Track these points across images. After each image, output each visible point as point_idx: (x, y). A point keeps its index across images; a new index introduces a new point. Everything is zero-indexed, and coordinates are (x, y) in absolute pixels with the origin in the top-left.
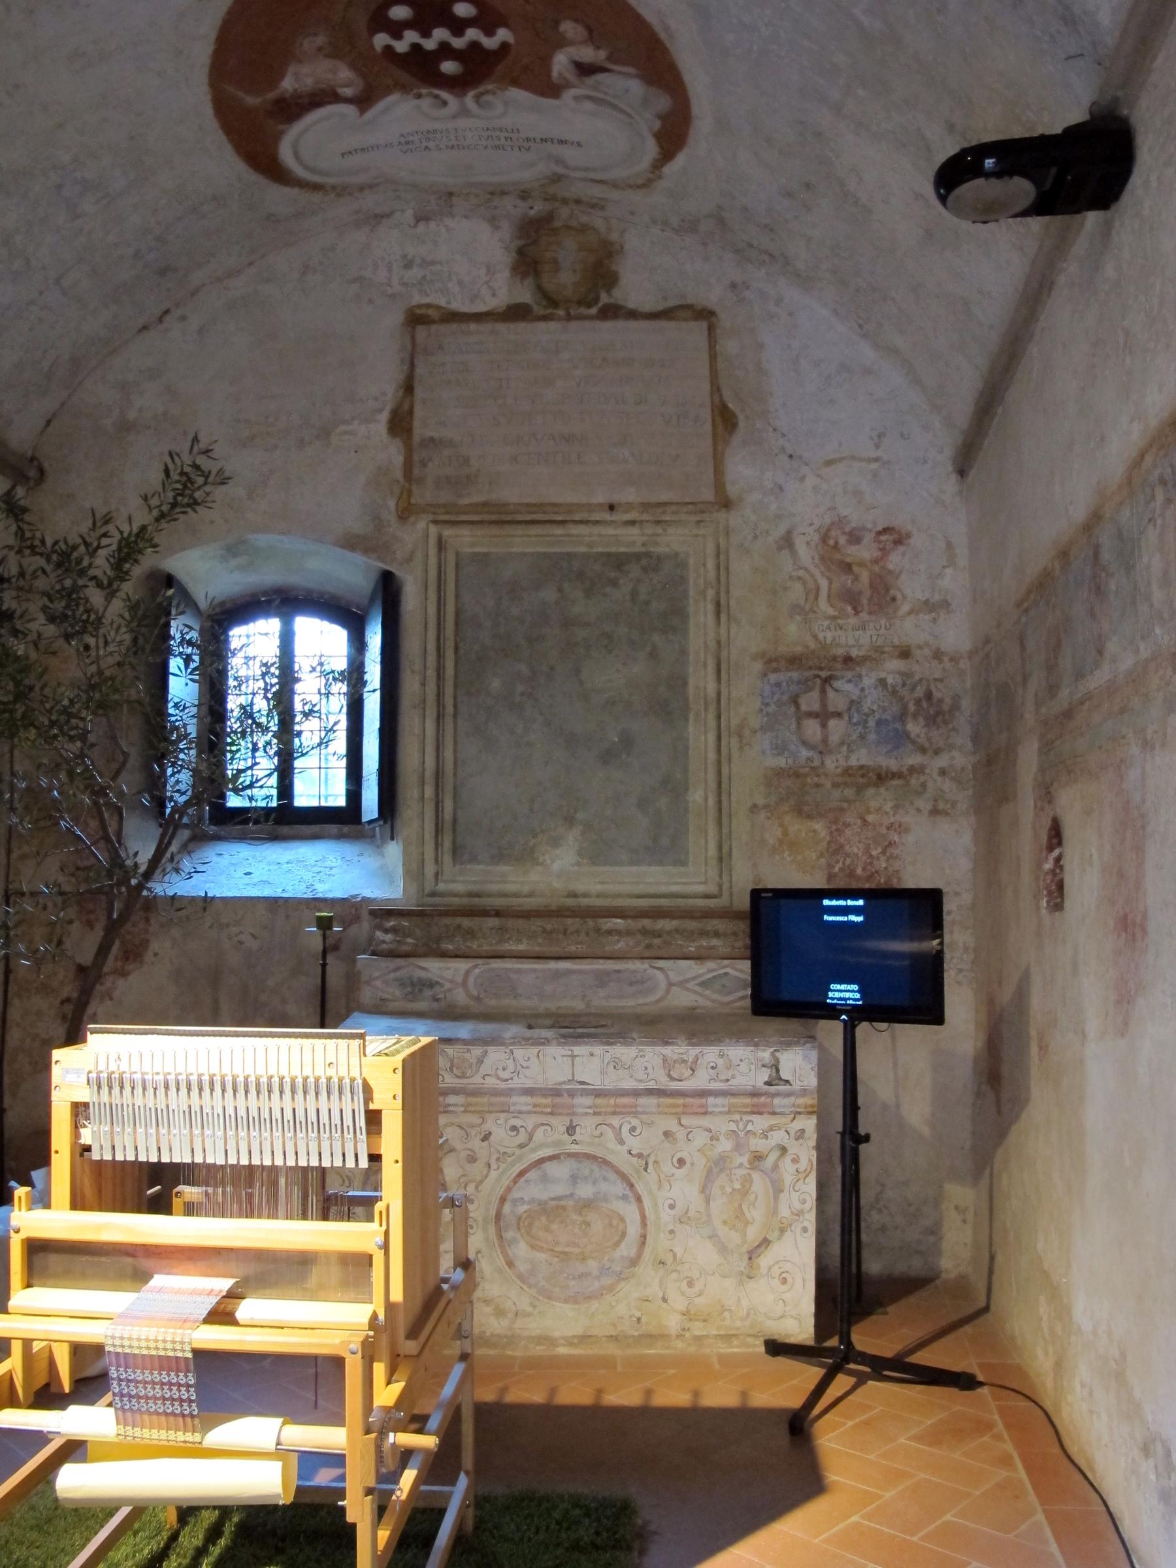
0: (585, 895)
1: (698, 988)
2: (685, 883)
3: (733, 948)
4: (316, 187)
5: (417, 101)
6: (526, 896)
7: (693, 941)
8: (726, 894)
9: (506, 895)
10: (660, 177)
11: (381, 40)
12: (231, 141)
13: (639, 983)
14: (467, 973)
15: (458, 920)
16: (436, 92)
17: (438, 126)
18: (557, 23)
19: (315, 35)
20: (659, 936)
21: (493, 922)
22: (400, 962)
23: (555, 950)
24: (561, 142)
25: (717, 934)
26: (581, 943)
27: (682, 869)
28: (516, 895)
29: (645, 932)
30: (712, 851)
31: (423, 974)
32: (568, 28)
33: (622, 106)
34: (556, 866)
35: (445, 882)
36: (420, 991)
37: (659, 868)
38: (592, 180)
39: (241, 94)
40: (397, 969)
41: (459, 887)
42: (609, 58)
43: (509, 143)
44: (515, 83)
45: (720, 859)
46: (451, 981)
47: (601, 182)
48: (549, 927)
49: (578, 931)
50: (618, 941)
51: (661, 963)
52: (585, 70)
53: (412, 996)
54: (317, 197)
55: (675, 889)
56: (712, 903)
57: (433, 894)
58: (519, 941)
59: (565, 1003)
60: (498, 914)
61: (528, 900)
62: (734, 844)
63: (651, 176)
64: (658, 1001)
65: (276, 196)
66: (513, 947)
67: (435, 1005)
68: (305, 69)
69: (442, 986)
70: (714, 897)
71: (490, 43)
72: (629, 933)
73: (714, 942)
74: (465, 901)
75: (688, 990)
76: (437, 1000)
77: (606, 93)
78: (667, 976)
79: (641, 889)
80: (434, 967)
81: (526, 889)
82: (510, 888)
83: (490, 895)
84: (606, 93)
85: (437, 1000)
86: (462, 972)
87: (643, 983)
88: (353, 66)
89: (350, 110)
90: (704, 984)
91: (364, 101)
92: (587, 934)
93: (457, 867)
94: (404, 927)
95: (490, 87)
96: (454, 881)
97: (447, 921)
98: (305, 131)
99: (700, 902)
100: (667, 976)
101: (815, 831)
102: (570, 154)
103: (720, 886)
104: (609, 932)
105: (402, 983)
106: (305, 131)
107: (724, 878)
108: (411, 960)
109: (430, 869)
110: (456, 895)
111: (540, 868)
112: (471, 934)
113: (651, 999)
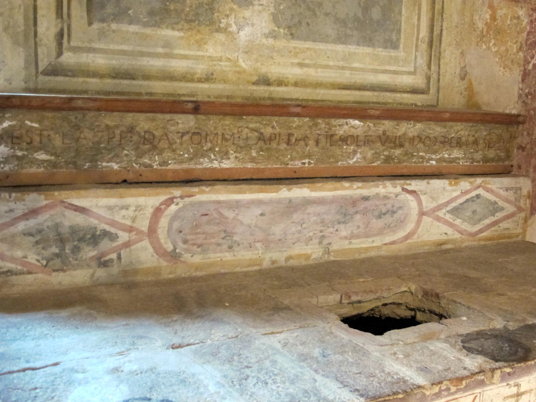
0: (280, 83)
1: (448, 217)
2: (395, 73)
3: (473, 160)
6: (200, 81)
7: (435, 152)
8: (432, 91)
9: (170, 77)
13: (390, 212)
14: (158, 212)
15: (130, 118)
20: (401, 146)
21: (186, 122)
22: (35, 200)
23: (272, 166)
25: (459, 144)
26: (309, 156)
27: (393, 53)
28: (186, 78)
29: (386, 140)
30: (424, 33)
31: (79, 220)
34: (244, 35)
35: (76, 50)
36: (76, 250)
37: (368, 50)
40: (34, 212)
41: (100, 61)
45: (431, 44)
46: (130, 229)
48: (268, 131)
49: (305, 138)
50: (355, 152)
51: (415, 185)
53: (61, 262)
55: (384, 79)
56: (419, 99)
57: (54, 71)
58: (225, 155)
59: (298, 250)
60: (196, 108)
61: (206, 86)
62: (445, 25)
64: (407, 238)
66: (216, 165)
67: (101, 273)
69: (113, 237)
70: (422, 92)
72: (368, 141)
73: (457, 153)
74: (109, 84)
75: (438, 219)
76: (105, 264)
78: (420, 203)
79: (346, 77)
80: (100, 206)
81: (200, 68)
82: (178, 66)
83: (147, 77)
85: (105, 264)
86: (149, 211)
87: (394, 212)
90: (455, 211)
92: (317, 142)
93: (96, 26)
94: (30, 129)
96: (90, 50)
97: (109, 120)
99: (408, 98)
100: (420, 203)
101: (518, 18)
103: (428, 78)
104: (344, 140)
105: (39, 237)
107: (433, 67)
108: (57, 194)
109: (47, 27)
110: (95, 74)
111: (221, 37)
112: (149, 143)
113: (401, 234)
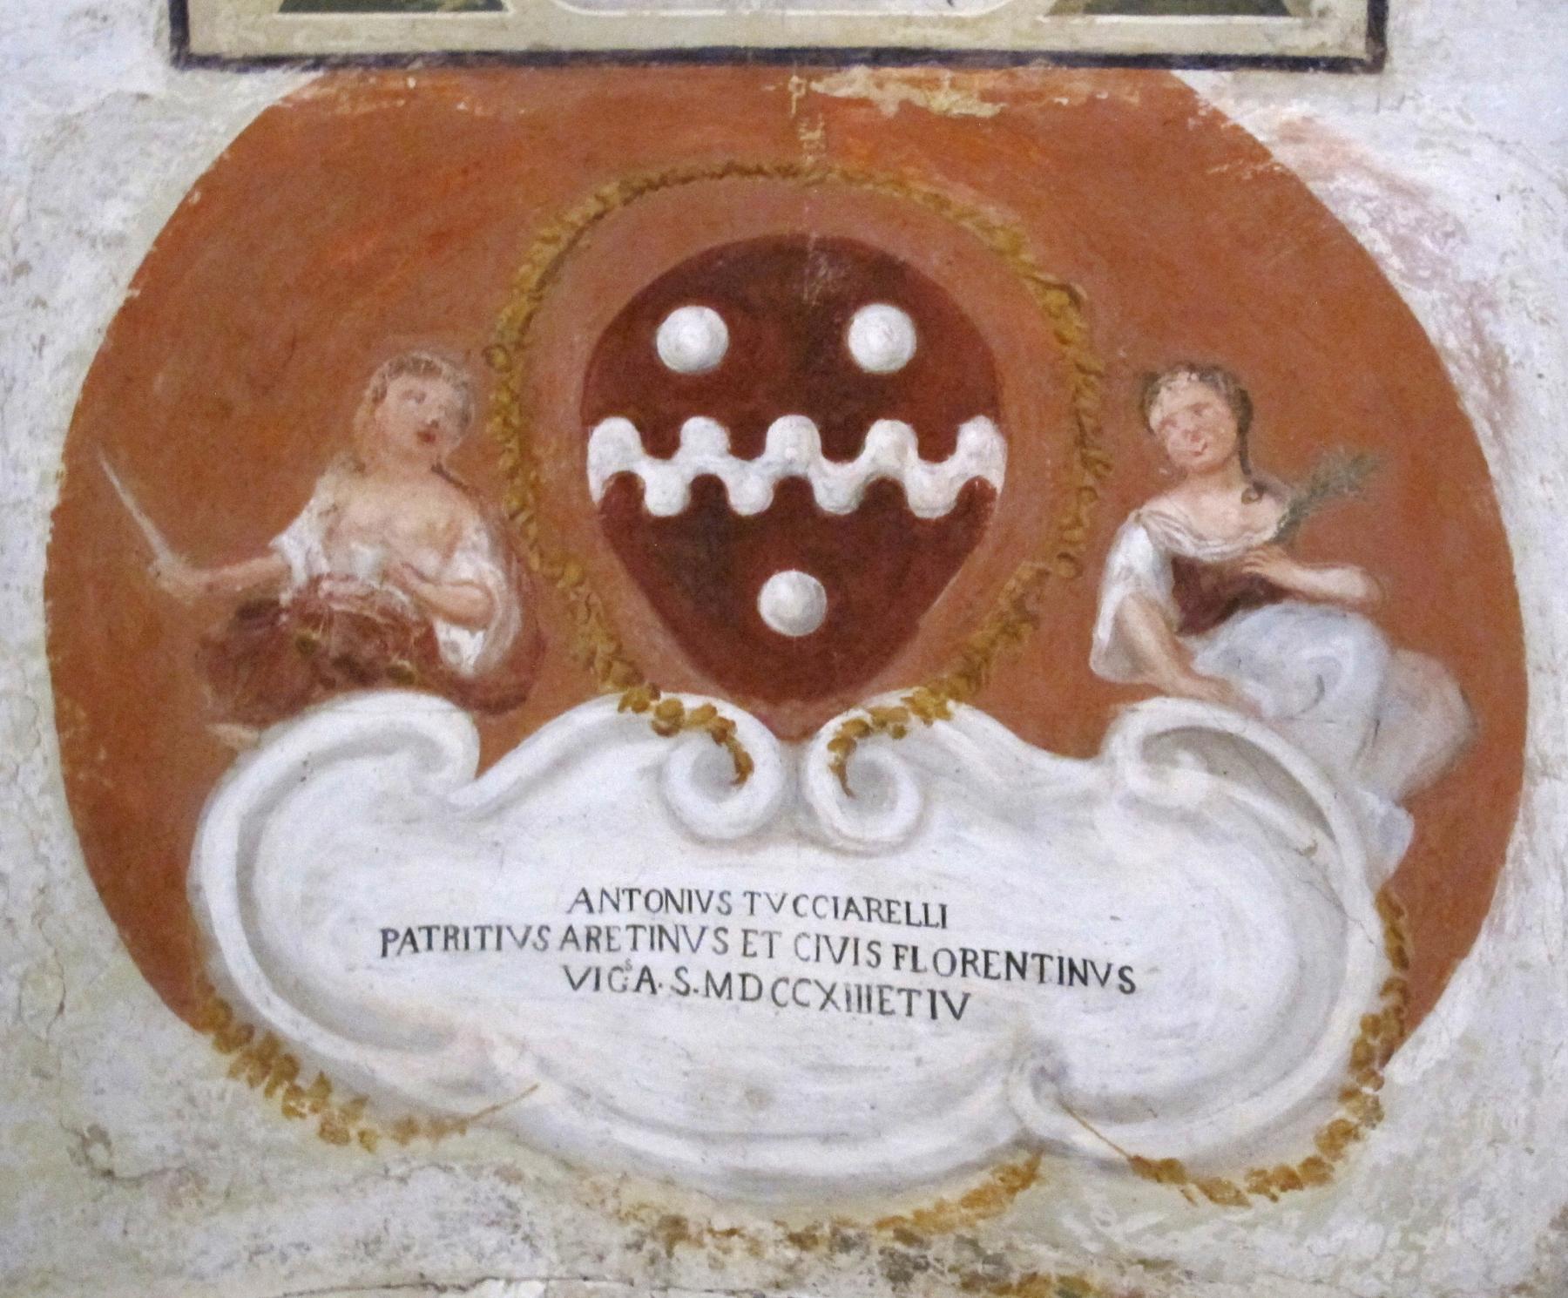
4: (270, 1061)
5: (660, 746)
10: (1374, 1113)
11: (614, 444)
12: (62, 721)
16: (728, 710)
17: (706, 874)
18: (1149, 383)
19: (430, 371)
24: (1074, 973)
32: (1185, 408)
33: (1301, 770)
38: (1143, 1167)
39: (155, 539)
42: (1289, 541)
43: (905, 978)
44: (974, 683)
47: (1166, 1171)
52: (1207, 596)
54: (258, 1112)
63: (1342, 1113)
65: (146, 1060)
68: (366, 504)
71: (930, 489)
77: (1252, 711)
84: (1252, 711)
88: (507, 545)
89: (446, 726)
91: (504, 706)
95: (892, 700)
98: (302, 773)
102: (1084, 1029)
106: (302, 773)
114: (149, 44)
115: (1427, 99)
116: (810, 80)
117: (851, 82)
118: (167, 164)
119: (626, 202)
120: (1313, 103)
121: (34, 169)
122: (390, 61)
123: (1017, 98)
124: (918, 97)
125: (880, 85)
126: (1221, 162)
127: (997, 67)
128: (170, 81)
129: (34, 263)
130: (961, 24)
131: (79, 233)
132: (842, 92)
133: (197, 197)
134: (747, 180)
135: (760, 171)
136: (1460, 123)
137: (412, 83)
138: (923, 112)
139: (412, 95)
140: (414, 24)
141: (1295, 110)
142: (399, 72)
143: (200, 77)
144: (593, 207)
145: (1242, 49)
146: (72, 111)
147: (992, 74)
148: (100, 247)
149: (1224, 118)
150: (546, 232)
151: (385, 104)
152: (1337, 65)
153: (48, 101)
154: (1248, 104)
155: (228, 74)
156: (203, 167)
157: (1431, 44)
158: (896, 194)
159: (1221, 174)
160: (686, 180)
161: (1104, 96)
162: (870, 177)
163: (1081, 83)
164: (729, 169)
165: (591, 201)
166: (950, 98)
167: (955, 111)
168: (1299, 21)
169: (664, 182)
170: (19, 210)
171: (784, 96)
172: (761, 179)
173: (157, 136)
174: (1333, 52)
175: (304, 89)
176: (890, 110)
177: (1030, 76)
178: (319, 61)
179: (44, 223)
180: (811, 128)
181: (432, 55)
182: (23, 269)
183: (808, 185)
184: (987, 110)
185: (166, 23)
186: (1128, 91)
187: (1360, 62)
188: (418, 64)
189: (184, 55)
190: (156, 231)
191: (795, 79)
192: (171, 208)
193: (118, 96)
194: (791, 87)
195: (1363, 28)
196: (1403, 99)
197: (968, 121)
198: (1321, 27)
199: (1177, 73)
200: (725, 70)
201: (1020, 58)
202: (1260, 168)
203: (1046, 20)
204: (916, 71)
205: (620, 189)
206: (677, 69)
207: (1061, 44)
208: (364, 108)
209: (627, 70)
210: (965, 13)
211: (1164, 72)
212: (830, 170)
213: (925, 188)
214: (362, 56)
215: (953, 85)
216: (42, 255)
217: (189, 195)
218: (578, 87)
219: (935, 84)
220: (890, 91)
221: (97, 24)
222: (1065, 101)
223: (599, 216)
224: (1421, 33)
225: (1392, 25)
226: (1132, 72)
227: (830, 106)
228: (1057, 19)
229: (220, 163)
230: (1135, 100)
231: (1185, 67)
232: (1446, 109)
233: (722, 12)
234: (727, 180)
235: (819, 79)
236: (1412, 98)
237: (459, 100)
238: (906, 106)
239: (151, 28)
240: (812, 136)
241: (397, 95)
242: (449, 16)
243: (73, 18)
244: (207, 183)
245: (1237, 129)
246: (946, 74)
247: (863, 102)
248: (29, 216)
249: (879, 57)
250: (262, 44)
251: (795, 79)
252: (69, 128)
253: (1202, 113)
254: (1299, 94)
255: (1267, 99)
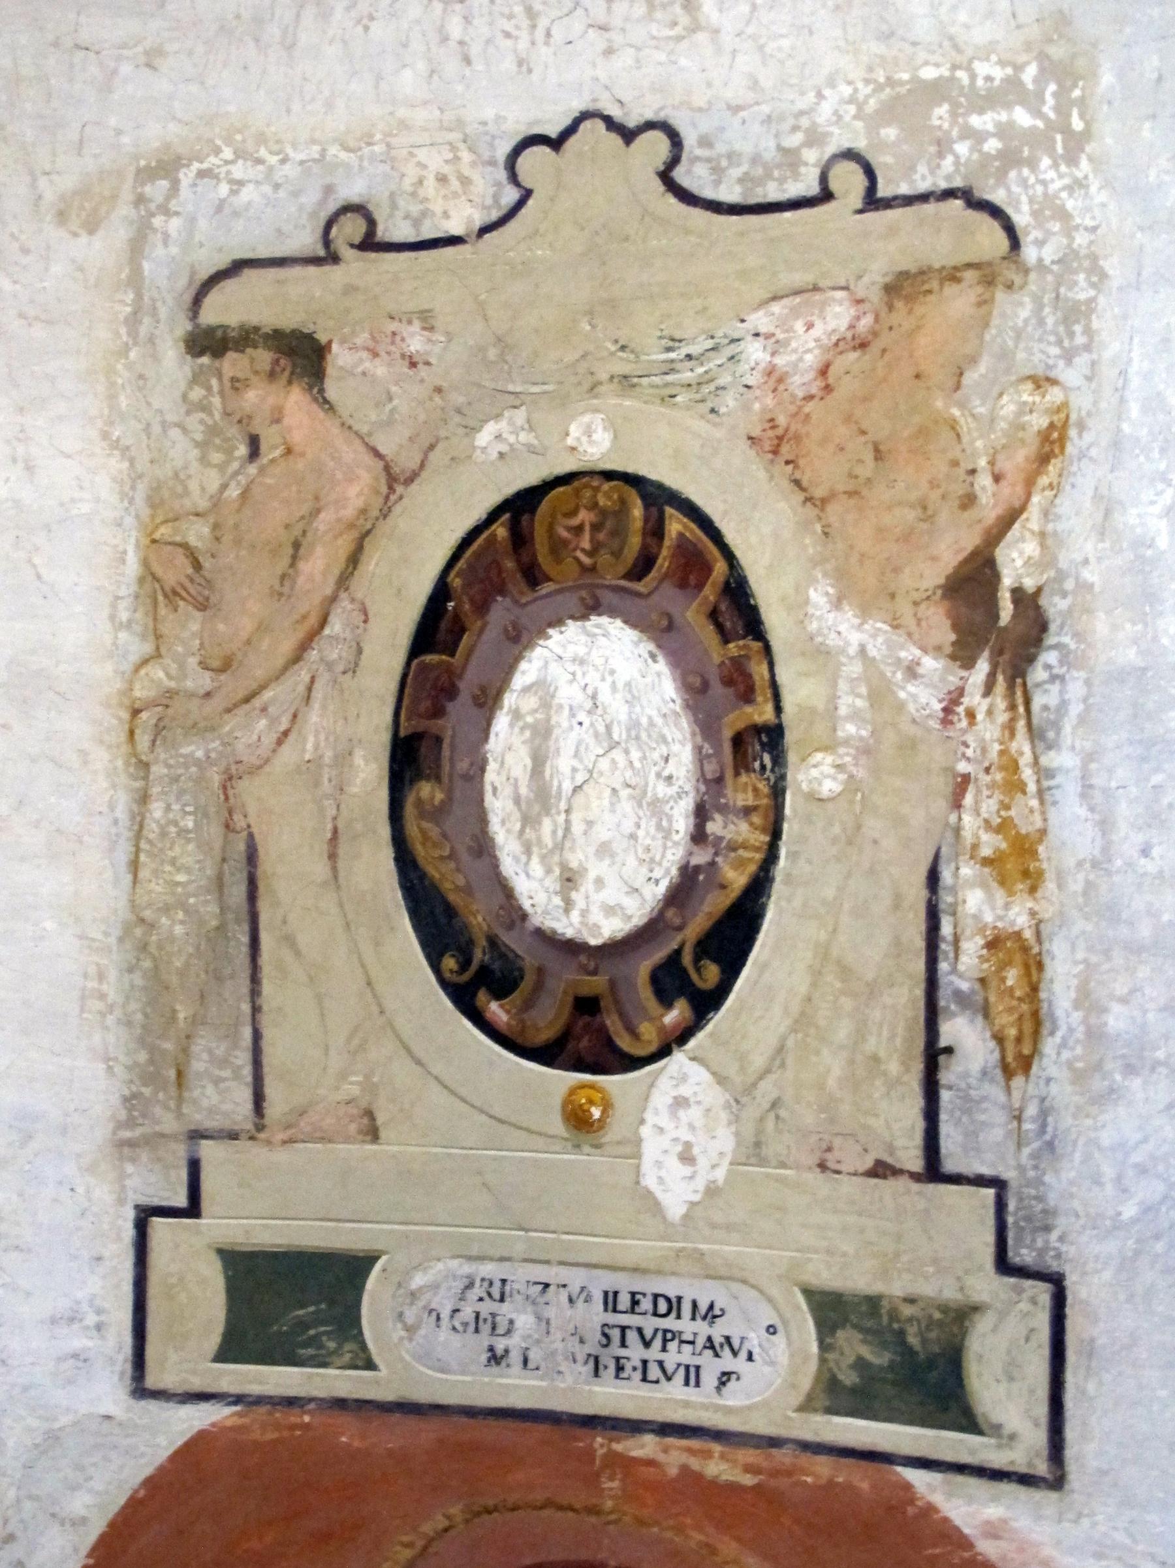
114: (116, 1378)
115: (1100, 1517)
116: (611, 1440)
117: (642, 1447)
118: (122, 1467)
119: (467, 1521)
120: (1008, 1508)
121: (25, 1467)
122: (291, 1402)
123: (775, 1473)
124: (695, 1464)
125: (666, 1451)
126: (935, 1546)
127: (757, 1447)
128: (129, 1409)
129: (18, 1534)
130: (729, 1411)
131: (53, 1515)
132: (636, 1453)
133: (142, 1493)
134: (560, 1514)
135: (572, 1509)
136: (1128, 1541)
137: (307, 1419)
138: (698, 1477)
139: (306, 1427)
140: (310, 1376)
141: (993, 1512)
142: (297, 1410)
143: (152, 1405)
144: (442, 1523)
145: (949, 1457)
146: (57, 1425)
147: (751, 1451)
148: (67, 1526)
149: (937, 1511)
150: (405, 1539)
151: (286, 1434)
152: (1026, 1480)
153: (39, 1417)
154: (957, 1502)
155: (171, 1405)
156: (148, 1471)
157: (1103, 1473)
158: (677, 1539)
159: (936, 1556)
160: (514, 1509)
161: (840, 1480)
162: (657, 1523)
163: (823, 1467)
164: (548, 1504)
165: (440, 1517)
166: (719, 1467)
167: (724, 1477)
168: (993, 1441)
169: (496, 1509)
170: (12, 1493)
171: (590, 1453)
172: (570, 1514)
173: (115, 1447)
174: (1023, 1470)
175: (227, 1417)
176: (673, 1471)
177: (784, 1457)
178: (238, 1399)
179: (28, 1505)
180: (612, 1479)
181: (321, 1400)
182: (11, 1538)
183: (609, 1523)
184: (748, 1480)
185: (129, 1367)
186: (860, 1478)
187: (1043, 1479)
188: (312, 1406)
189: (141, 1390)
190: (110, 1516)
191: (599, 1439)
192: (122, 1501)
193: (89, 1416)
194: (596, 1445)
195: (1045, 1453)
196: (1080, 1515)
197: (733, 1488)
198: (1011, 1449)
199: (899, 1469)
200: (544, 1428)
201: (774, 1442)
202: (966, 1555)
203: (794, 1415)
204: (694, 1443)
205: (463, 1511)
206: (511, 1424)
207: (808, 1436)
208: (271, 1436)
209: (472, 1421)
210: (730, 1403)
211: (886, 1466)
212: (625, 1514)
213: (701, 1537)
214: (271, 1397)
215: (723, 1456)
216: (26, 1529)
217: (136, 1491)
218: (428, 1432)
219: (707, 1455)
220: (674, 1456)
221: (80, 1364)
222: (809, 1480)
223: (446, 1530)
224: (1093, 1464)
225: (1070, 1453)
226: (863, 1463)
227: (628, 1464)
228: (804, 1415)
229: (162, 1470)
230: (865, 1486)
231: (904, 1465)
232: (1115, 1528)
233: (544, 1384)
234: (546, 1513)
235: (618, 1441)
236: (1088, 1515)
237: (343, 1434)
238: (685, 1469)
239: (118, 1368)
240: (612, 1485)
241: (292, 1427)
242: (337, 1372)
243: (60, 1360)
244: (150, 1483)
245: (946, 1520)
246: (717, 1448)
247: (650, 1463)
248: (18, 1501)
249: (666, 1429)
250: (197, 1384)
251: (599, 1439)
252: (53, 1438)
253: (919, 1503)
254: (995, 1499)
255: (970, 1500)
